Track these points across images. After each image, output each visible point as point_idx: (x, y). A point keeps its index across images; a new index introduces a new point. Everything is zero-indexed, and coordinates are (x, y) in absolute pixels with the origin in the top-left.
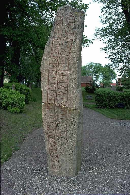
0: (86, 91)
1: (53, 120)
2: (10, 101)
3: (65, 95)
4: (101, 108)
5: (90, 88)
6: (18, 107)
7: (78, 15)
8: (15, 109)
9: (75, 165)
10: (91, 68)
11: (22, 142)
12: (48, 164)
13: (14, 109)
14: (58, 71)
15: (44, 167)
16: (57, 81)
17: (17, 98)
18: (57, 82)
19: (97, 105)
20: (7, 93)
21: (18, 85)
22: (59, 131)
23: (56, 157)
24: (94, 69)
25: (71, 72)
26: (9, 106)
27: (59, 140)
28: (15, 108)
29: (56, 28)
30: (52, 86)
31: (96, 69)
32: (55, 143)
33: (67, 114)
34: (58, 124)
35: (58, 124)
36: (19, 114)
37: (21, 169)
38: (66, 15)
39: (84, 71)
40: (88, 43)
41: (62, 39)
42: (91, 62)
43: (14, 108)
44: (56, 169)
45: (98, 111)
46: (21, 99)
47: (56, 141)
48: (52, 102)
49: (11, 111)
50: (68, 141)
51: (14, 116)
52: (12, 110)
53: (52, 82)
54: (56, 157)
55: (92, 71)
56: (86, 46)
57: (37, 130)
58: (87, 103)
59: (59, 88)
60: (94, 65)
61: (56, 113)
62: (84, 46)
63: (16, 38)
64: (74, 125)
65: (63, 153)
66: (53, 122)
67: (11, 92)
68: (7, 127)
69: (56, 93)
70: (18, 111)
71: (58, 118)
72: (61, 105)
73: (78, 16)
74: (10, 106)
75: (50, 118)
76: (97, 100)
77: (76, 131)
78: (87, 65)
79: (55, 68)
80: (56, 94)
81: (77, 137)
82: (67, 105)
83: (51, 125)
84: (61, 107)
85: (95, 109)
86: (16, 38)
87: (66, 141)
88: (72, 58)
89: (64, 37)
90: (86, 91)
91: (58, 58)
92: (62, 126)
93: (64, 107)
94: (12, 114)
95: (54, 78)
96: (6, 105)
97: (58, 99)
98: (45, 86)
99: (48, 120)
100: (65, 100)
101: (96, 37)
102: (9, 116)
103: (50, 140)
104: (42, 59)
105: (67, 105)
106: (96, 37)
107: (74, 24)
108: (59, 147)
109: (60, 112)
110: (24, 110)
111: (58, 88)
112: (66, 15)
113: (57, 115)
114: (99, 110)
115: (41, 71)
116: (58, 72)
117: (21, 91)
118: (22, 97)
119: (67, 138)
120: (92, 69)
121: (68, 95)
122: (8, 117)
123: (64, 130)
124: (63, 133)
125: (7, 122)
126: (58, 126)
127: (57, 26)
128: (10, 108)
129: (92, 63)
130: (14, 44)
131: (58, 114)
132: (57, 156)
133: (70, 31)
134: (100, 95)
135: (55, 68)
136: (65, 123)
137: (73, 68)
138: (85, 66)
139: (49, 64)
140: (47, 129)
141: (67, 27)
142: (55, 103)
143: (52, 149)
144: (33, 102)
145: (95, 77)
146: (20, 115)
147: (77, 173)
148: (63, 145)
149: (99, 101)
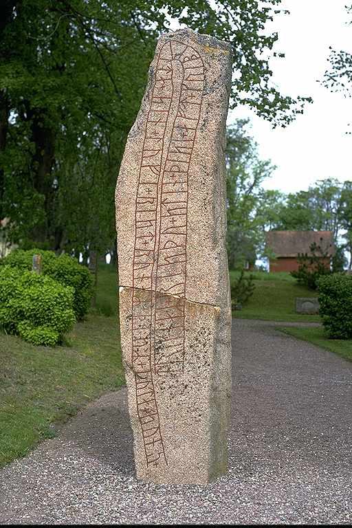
0: (299, 285)
1: (148, 331)
2: (26, 305)
3: (179, 266)
4: (339, 338)
5: (311, 272)
6: (53, 326)
7: (213, 55)
8: (44, 332)
9: (205, 454)
10: (329, 200)
11: (65, 421)
12: (136, 452)
13: (39, 330)
14: (162, 203)
15: (126, 465)
16: (158, 229)
17: (47, 297)
18: (158, 232)
19: (327, 329)
20: (17, 281)
21: (51, 257)
22: (164, 360)
23: (155, 430)
24: (340, 202)
25: (193, 206)
26: (23, 322)
27: (164, 385)
28: (43, 330)
29: (156, 91)
30: (146, 243)
31: (348, 204)
32: (153, 392)
33: (184, 316)
34: (161, 342)
35: (161, 342)
36: (54, 347)
37: (63, 471)
38: (181, 54)
39: (299, 212)
40: (288, 113)
41: (171, 119)
42: (327, 178)
43: (40, 328)
44: (156, 464)
45: (330, 347)
46: (60, 301)
47: (156, 390)
48: (146, 284)
49: (29, 336)
50: (186, 386)
51: (41, 353)
52: (31, 333)
53: (146, 231)
54: (155, 430)
55: (334, 211)
56: (283, 126)
57: (113, 393)
58: (296, 324)
59: (164, 248)
60: (341, 186)
61: (155, 315)
62: (275, 125)
63: (41, 99)
64: (204, 345)
65: (175, 419)
66: (147, 338)
67: (28, 277)
68: (19, 380)
69: (156, 260)
70: (50, 338)
71: (162, 327)
72: (171, 292)
73: (213, 57)
74: (25, 324)
75: (140, 326)
76: (326, 309)
77: (210, 360)
78: (314, 187)
79: (153, 194)
80: (155, 265)
81: (213, 378)
82: (184, 293)
83: (142, 344)
84: (169, 297)
85: (318, 341)
86: (43, 99)
87: (181, 387)
88: (196, 168)
89: (175, 112)
90: (299, 285)
91: (160, 169)
92: (172, 348)
93: (175, 296)
94: (31, 348)
95: (150, 221)
96: (14, 319)
97: (161, 277)
98: (126, 242)
99: (135, 332)
100: (179, 279)
101: (330, 86)
102: (23, 353)
103: (139, 386)
104: (120, 173)
105: (184, 293)
106: (330, 86)
107: (202, 77)
108: (163, 400)
109: (166, 309)
110: (71, 337)
111: (162, 246)
112: (181, 54)
113: (157, 319)
114: (330, 344)
115: (117, 204)
116: (161, 207)
117: (60, 277)
118: (62, 294)
119: (185, 378)
120: (333, 202)
121: (188, 266)
122: (21, 354)
123: (177, 358)
124: (174, 367)
125: (17, 369)
126: (160, 347)
127: (158, 85)
128: (26, 329)
129: (333, 182)
130: (32, 115)
131: (163, 317)
132: (159, 427)
133: (192, 96)
134: (335, 294)
135: (153, 194)
136: (179, 340)
137: (200, 196)
138: (307, 190)
139: (138, 186)
140: (131, 355)
141: (184, 87)
142: (154, 289)
143: (145, 410)
144: (102, 317)
145: (343, 236)
146: (60, 351)
147: (212, 477)
148: (173, 397)
149: (333, 314)
